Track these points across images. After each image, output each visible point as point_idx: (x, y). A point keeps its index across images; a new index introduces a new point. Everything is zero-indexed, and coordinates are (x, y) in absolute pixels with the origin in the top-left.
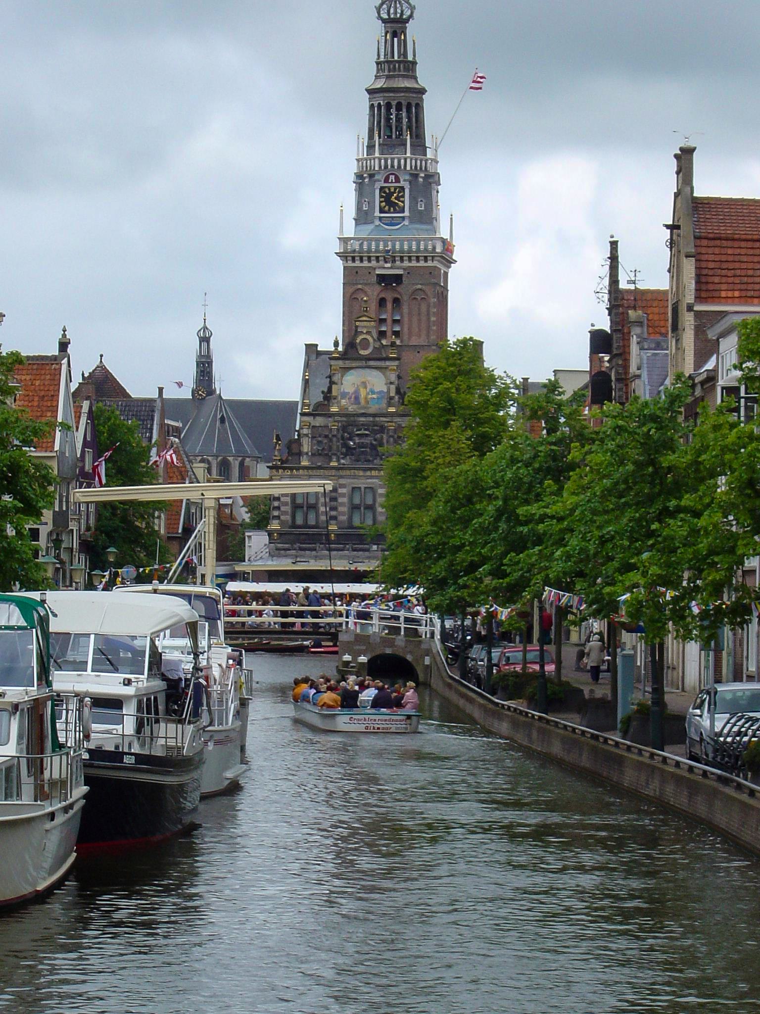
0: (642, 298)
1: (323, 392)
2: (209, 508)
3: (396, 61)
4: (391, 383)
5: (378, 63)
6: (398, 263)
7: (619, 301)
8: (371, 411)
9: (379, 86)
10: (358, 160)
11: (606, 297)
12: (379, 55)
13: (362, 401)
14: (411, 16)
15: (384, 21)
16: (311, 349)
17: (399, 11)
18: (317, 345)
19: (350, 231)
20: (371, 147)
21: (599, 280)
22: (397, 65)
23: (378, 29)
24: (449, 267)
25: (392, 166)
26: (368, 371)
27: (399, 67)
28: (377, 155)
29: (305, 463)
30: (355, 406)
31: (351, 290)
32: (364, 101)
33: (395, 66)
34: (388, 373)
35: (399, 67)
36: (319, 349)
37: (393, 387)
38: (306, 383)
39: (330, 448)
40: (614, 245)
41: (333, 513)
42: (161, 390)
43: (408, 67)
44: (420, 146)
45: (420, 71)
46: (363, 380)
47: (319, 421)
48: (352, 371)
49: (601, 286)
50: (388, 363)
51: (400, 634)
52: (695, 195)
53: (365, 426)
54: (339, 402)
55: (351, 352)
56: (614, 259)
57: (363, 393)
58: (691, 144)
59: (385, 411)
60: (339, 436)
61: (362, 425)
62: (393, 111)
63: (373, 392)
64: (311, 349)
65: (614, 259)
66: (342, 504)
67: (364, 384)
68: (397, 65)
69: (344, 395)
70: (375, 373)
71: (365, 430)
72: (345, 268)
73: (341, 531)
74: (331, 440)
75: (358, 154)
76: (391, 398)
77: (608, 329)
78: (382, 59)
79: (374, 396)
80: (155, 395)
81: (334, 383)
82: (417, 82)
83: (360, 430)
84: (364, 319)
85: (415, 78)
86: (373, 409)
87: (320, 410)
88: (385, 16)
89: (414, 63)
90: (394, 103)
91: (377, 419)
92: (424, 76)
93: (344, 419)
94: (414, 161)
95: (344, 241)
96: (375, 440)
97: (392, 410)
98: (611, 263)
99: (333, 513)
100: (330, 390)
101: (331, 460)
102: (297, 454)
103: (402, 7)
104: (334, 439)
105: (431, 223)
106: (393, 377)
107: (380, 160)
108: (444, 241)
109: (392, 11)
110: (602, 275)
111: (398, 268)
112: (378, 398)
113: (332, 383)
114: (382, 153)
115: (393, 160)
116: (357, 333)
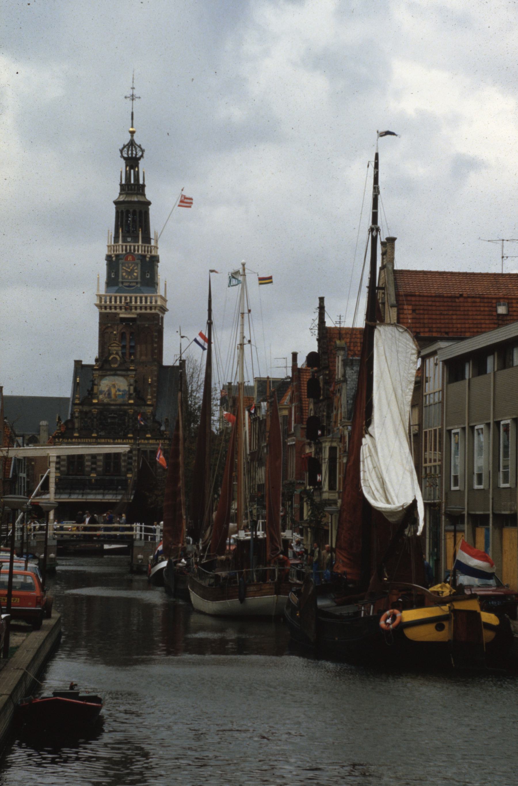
0: (340, 333)
1: (88, 390)
4: (131, 385)
6: (133, 311)
13: (113, 396)
14: (142, 156)
15: (125, 158)
16: (78, 363)
17: (134, 152)
18: (81, 361)
19: (103, 290)
23: (122, 163)
24: (164, 313)
26: (116, 377)
27: (135, 188)
28: (120, 243)
30: (108, 400)
31: (104, 327)
34: (129, 379)
35: (135, 188)
36: (83, 363)
40: (322, 300)
41: (94, 466)
43: (140, 189)
44: (147, 239)
46: (114, 383)
47: (86, 409)
48: (107, 378)
49: (313, 325)
50: (129, 373)
57: (113, 391)
58: (392, 235)
59: (127, 403)
63: (119, 390)
64: (78, 363)
66: (100, 461)
67: (114, 386)
69: (101, 392)
70: (121, 379)
71: (114, 414)
72: (101, 314)
73: (99, 478)
76: (130, 394)
79: (121, 393)
81: (96, 385)
83: (111, 414)
86: (120, 401)
88: (126, 156)
89: (143, 186)
91: (122, 407)
92: (149, 194)
93: (101, 407)
94: (143, 248)
95: (100, 297)
97: (131, 401)
98: (320, 311)
99: (94, 466)
100: (92, 389)
105: (154, 287)
106: (132, 381)
108: (161, 297)
109: (130, 152)
111: (133, 314)
112: (123, 394)
113: (94, 385)
115: (130, 246)
116: (110, 354)
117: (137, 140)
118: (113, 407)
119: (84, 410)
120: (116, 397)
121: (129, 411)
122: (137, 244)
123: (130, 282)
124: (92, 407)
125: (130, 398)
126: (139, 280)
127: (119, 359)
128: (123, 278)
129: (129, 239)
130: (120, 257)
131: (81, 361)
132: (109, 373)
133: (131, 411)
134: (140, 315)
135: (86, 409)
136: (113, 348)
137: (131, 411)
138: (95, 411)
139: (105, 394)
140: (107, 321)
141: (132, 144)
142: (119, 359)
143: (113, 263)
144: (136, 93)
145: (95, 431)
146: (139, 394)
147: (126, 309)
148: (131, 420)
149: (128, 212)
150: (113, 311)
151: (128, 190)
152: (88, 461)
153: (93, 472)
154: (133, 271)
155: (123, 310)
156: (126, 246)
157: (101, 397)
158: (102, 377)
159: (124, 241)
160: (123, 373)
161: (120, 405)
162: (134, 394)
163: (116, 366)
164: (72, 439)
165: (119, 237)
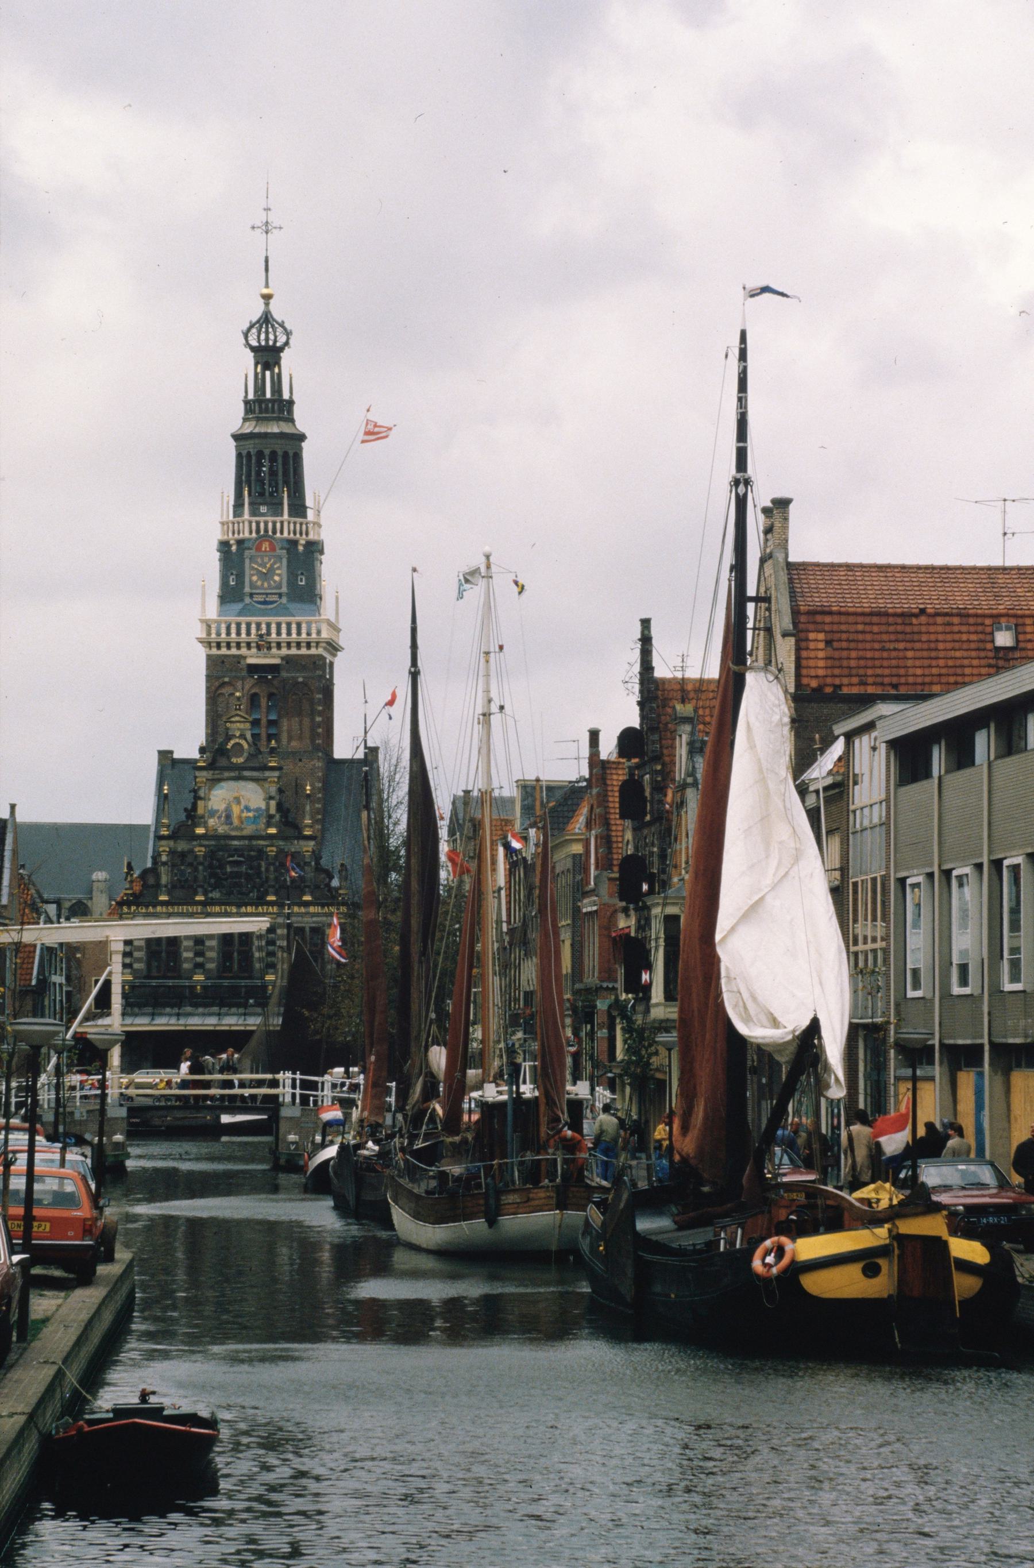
0: (683, 689)
1: (186, 810)
2: (117, 952)
3: (269, 400)
4: (271, 798)
5: (246, 402)
6: (274, 651)
7: (653, 693)
8: (245, 833)
9: (248, 431)
10: (223, 524)
11: (637, 688)
12: (246, 392)
13: (236, 822)
14: (287, 343)
15: (253, 349)
16: (165, 757)
17: (271, 337)
18: (171, 752)
19: (212, 610)
20: (238, 506)
21: (627, 667)
22: (269, 405)
24: (335, 655)
25: (266, 530)
26: (242, 783)
28: (246, 516)
29: (163, 898)
30: (226, 827)
32: (230, 450)
33: (267, 406)
34: (267, 785)
36: (176, 756)
37: (273, 803)
38: (162, 799)
39: (196, 879)
40: (646, 623)
41: (199, 960)
42: (13, 807)
43: (283, 408)
44: (299, 509)
45: (298, 412)
46: (236, 794)
47: (182, 846)
48: (223, 784)
49: (630, 674)
50: (267, 774)
51: (309, 1105)
52: (790, 559)
53: (237, 851)
54: (206, 823)
55: (217, 757)
56: (646, 641)
57: (236, 810)
60: (206, 864)
61: (236, 850)
62: (266, 462)
63: (248, 809)
64: (165, 757)
65: (646, 641)
67: (237, 800)
68: (269, 405)
69: (212, 813)
70: (251, 785)
72: (209, 657)
73: (209, 983)
74: (196, 870)
75: (222, 516)
76: (270, 817)
77: (637, 726)
78: (251, 396)
79: (251, 814)
80: (5, 815)
81: (201, 798)
82: (294, 425)
83: (233, 856)
84: (237, 719)
85: (292, 421)
87: (182, 831)
88: (255, 343)
89: (291, 403)
90: (267, 452)
91: (254, 843)
92: (303, 420)
93: (213, 843)
96: (251, 868)
97: (273, 831)
99: (199, 960)
101: (196, 894)
102: (153, 886)
103: (275, 332)
104: (201, 868)
106: (273, 790)
107: (250, 523)
109: (263, 336)
110: (632, 661)
111: (274, 657)
112: (255, 817)
114: (290, 515)
116: (229, 738)
117: (278, 312)
118: (236, 843)
119: (179, 849)
120: (242, 823)
121: (269, 849)
122: (278, 519)
123: (267, 594)
124: (195, 843)
125: (269, 825)
126: (284, 589)
127: (246, 746)
128: (252, 585)
129: (263, 509)
130: (246, 545)
131: (171, 752)
132: (226, 774)
133: (272, 851)
134: (287, 659)
135: (182, 846)
136: (234, 726)
137: (272, 851)
138: (200, 851)
139: (219, 817)
140: (222, 673)
141: (266, 320)
142: (246, 746)
143: (232, 556)
144: (274, 219)
145: (200, 890)
146: (287, 818)
147: (259, 647)
148: (272, 868)
149: (260, 454)
150: (234, 651)
151: (261, 412)
152: (187, 950)
153: (197, 971)
154: (271, 571)
155: (254, 650)
156: (258, 523)
157: (211, 822)
158: (215, 782)
159: (254, 513)
160: (255, 774)
161: (250, 838)
162: (278, 817)
163: (241, 760)
164: (154, 906)
165: (243, 505)
